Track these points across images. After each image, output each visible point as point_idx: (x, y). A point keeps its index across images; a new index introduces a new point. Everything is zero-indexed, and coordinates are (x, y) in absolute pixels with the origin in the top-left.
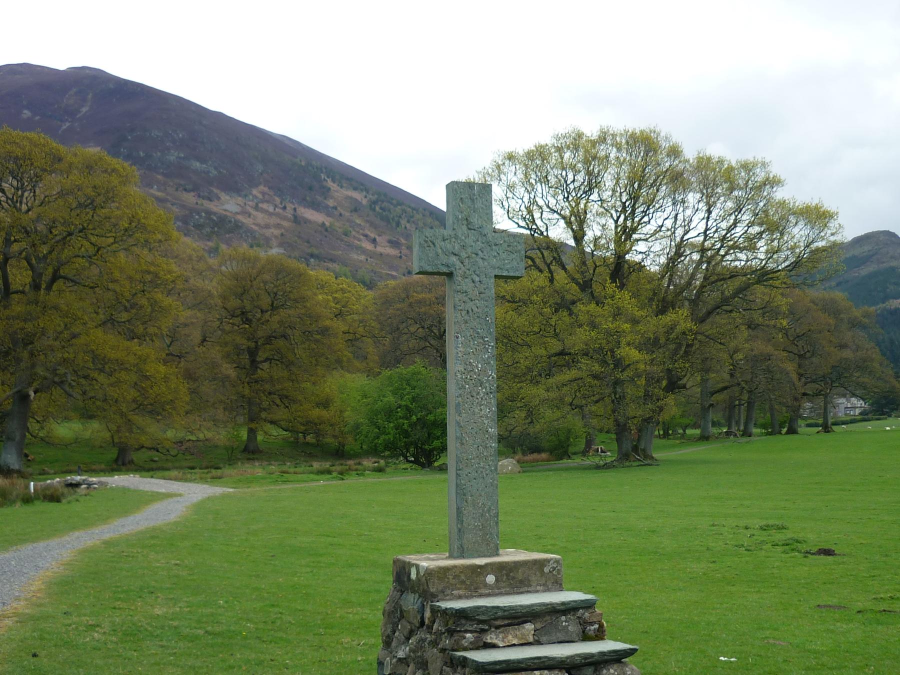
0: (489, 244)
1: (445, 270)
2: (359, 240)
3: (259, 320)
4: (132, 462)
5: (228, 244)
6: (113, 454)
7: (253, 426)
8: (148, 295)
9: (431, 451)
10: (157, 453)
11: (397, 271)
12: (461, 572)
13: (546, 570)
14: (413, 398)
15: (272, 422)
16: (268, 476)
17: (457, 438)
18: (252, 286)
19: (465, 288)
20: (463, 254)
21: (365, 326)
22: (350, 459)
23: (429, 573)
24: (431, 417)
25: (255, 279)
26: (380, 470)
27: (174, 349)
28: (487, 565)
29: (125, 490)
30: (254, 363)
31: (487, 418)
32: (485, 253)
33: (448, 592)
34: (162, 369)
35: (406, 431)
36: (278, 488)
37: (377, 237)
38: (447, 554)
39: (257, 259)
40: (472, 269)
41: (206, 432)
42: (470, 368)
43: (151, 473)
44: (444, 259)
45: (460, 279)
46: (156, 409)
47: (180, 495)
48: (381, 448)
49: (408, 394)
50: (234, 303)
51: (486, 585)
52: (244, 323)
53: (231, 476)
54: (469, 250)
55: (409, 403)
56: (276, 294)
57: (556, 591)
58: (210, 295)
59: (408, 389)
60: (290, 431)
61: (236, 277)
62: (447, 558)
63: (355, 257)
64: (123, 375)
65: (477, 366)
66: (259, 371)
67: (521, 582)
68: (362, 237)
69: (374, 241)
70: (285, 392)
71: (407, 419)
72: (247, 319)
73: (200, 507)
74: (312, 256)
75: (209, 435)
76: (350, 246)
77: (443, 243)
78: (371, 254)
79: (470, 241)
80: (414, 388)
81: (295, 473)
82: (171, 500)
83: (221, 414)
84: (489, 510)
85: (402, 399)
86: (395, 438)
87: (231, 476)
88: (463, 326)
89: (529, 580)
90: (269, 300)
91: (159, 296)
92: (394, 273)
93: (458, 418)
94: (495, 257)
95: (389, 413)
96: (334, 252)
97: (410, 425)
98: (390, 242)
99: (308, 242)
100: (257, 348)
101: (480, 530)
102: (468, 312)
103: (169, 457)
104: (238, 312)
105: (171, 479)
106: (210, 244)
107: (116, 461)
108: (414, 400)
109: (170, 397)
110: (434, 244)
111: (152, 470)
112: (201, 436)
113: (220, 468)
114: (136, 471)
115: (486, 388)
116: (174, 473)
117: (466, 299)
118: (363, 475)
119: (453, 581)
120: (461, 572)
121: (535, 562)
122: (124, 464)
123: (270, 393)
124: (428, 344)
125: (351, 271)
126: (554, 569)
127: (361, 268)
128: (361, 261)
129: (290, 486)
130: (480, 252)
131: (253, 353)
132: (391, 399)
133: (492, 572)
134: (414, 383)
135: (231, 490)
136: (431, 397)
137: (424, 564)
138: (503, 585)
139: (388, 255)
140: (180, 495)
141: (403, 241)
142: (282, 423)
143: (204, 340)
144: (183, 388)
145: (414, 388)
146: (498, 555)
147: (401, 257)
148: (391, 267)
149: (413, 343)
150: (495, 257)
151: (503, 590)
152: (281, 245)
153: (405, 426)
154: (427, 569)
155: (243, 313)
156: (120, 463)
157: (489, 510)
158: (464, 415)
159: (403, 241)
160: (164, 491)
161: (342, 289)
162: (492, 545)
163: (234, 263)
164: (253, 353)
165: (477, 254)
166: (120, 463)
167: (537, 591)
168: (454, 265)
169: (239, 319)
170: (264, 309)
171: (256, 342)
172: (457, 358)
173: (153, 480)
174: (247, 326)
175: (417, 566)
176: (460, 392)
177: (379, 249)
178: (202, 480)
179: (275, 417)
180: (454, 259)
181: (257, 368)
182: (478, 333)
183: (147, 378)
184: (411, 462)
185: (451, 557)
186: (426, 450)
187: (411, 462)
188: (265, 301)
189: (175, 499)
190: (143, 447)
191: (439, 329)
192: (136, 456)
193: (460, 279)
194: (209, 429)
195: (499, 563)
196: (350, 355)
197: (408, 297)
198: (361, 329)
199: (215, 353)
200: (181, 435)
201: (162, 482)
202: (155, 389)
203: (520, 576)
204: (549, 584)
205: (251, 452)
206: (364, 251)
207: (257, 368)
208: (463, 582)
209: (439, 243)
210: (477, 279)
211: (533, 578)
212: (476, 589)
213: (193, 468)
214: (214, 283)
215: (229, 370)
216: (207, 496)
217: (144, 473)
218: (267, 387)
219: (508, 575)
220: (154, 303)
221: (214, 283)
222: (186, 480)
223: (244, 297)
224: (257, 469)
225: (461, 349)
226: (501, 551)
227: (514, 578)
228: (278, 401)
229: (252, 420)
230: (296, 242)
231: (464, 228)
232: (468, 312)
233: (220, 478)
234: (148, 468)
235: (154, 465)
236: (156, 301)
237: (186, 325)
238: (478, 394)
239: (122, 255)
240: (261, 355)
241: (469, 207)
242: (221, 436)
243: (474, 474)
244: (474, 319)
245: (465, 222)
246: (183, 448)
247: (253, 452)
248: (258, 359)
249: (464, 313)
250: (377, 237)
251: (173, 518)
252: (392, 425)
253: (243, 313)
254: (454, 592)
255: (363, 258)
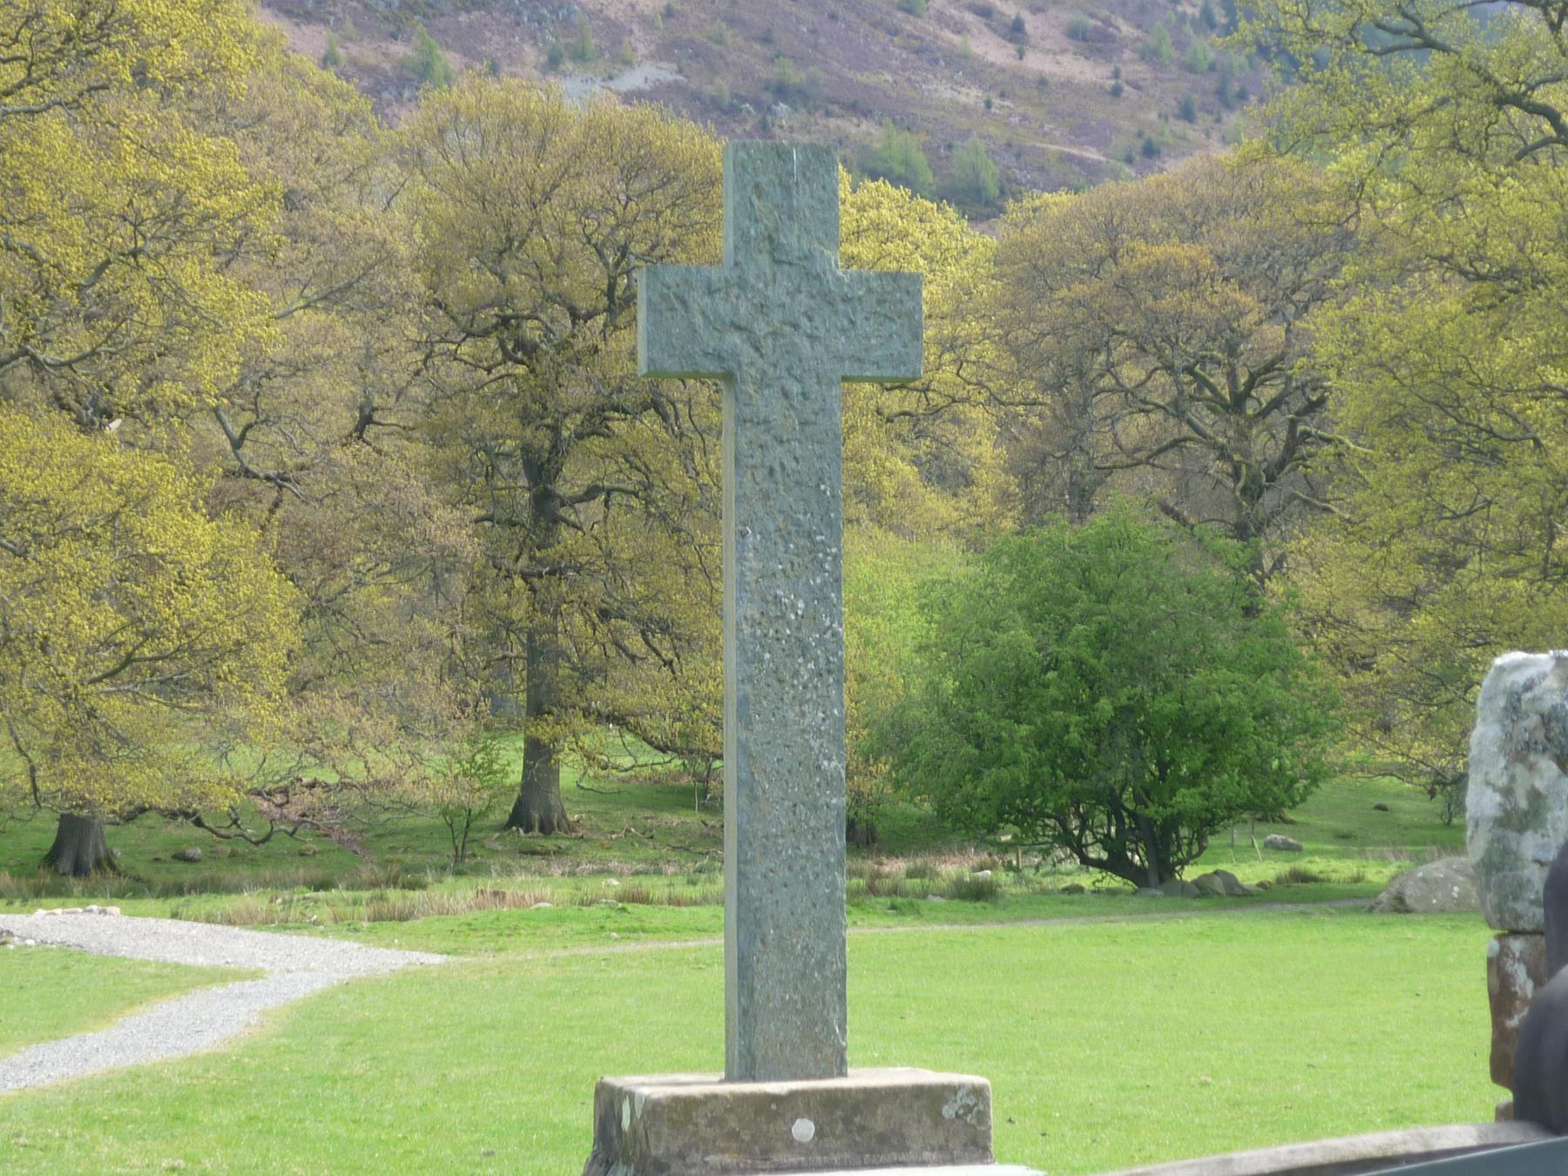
0: (826, 298)
1: (712, 366)
2: (960, 29)
3: (562, 346)
4: (106, 863)
5: (466, 52)
6: (44, 832)
7: (544, 732)
8: (151, 269)
9: (1171, 824)
10: (200, 832)
11: (1101, 143)
12: (731, 1110)
13: (948, 1111)
14: (1103, 633)
15: (618, 719)
16: (572, 911)
17: (740, 783)
18: (536, 222)
19: (763, 412)
20: (761, 328)
21: (960, 363)
22: (893, 854)
23: (655, 1109)
24: (1167, 705)
25: (547, 197)
26: (978, 893)
27: (260, 455)
28: (793, 1095)
29: (71, 954)
30: (545, 503)
31: (819, 733)
32: (817, 322)
33: (695, 1157)
34: (203, 530)
35: (1078, 754)
36: (603, 951)
37: (1026, 16)
38: (723, 1075)
39: (550, 126)
40: (783, 364)
41: (372, 755)
42: (773, 611)
43: (174, 902)
44: (710, 340)
45: (751, 389)
46: (184, 673)
47: (255, 975)
48: (986, 814)
49: (1085, 617)
50: (472, 281)
51: (791, 1144)
52: (508, 356)
53: (443, 911)
54: (776, 317)
55: (1086, 654)
56: (624, 251)
57: (971, 1161)
58: (387, 258)
59: (1085, 601)
60: (679, 752)
61: (481, 194)
62: (721, 1082)
63: (944, 92)
64: (67, 554)
65: (794, 607)
66: (565, 533)
67: (882, 1139)
68: (969, 17)
69: (1015, 32)
70: (660, 611)
71: (1081, 708)
72: (520, 344)
73: (313, 1018)
74: (782, 91)
75: (384, 764)
76: (926, 54)
77: (707, 300)
78: (1002, 84)
79: (778, 294)
80: (1106, 597)
81: (675, 902)
82: (217, 989)
83: (434, 696)
84: (821, 965)
85: (1061, 637)
86: (1035, 776)
87: (443, 911)
88: (758, 507)
89: (903, 1136)
90: (599, 276)
91: (189, 272)
92: (1092, 154)
93: (744, 735)
94: (843, 330)
95: (1017, 688)
96: (862, 78)
97: (1094, 732)
98: (1074, 33)
99: (766, 40)
100: (557, 448)
101: (798, 1012)
102: (771, 471)
103: (241, 847)
104: (489, 316)
105: (230, 922)
106: (399, 49)
107: (52, 858)
108: (1102, 640)
109: (235, 633)
110: (684, 303)
111: (179, 890)
112: (356, 771)
113: (423, 887)
114: (120, 894)
115: (816, 660)
116: (252, 900)
117: (766, 438)
118: (917, 912)
119: (708, 1133)
120: (731, 1110)
121: (919, 1092)
122: (79, 870)
123: (604, 615)
124: (1186, 429)
125: (926, 148)
126: (968, 1109)
127: (965, 135)
128: (965, 110)
129: (648, 946)
130: (804, 321)
131: (541, 470)
132: (1020, 636)
133: (807, 1113)
134: (1104, 580)
135: (437, 959)
136: (1168, 626)
137: (645, 1091)
138: (835, 1144)
139: (1067, 84)
140: (255, 975)
141: (1126, 29)
142: (646, 722)
143: (366, 420)
144: (279, 595)
145: (1106, 597)
146: (843, 1074)
147: (1116, 92)
148: (1082, 131)
149: (1135, 428)
150: (843, 330)
151: (836, 1159)
152: (665, 51)
153: (1074, 736)
154: (647, 1098)
155: (505, 321)
156: (66, 864)
157: (821, 965)
158: (759, 727)
159: (1126, 29)
160: (201, 960)
161: (877, 227)
162: (828, 1051)
163: (471, 141)
164: (541, 470)
165: (796, 326)
166: (66, 864)
167: (923, 1163)
168: (735, 355)
169: (493, 342)
170: (583, 306)
171: (555, 429)
172: (742, 585)
173: (181, 926)
174: (521, 370)
175: (631, 1095)
176: (752, 669)
177: (1036, 63)
178: (343, 924)
179: (628, 701)
180: (735, 339)
181: (556, 520)
182: (798, 524)
183: (153, 564)
184: (1098, 864)
185: (729, 1078)
186: (1150, 822)
187: (1098, 864)
188: (585, 278)
189: (235, 987)
190: (143, 810)
191: (1232, 376)
192: (120, 843)
193: (751, 389)
194: (381, 744)
195: (828, 1091)
196: (909, 472)
197: (1113, 254)
198: (948, 373)
199: (403, 464)
200: (283, 761)
201: (200, 929)
202: (183, 601)
203: (879, 1123)
204: (956, 1145)
205: (533, 822)
206: (976, 72)
207: (556, 520)
208: (733, 1135)
209: (698, 300)
210: (795, 388)
211: (913, 1132)
212: (766, 1154)
213: (324, 885)
214: (399, 216)
215: (454, 529)
216: (346, 977)
217: (150, 904)
218: (595, 588)
219: (847, 1121)
220: (172, 295)
221: (399, 216)
222: (284, 925)
223: (507, 262)
224: (542, 888)
225: (754, 564)
226: (850, 1070)
227: (862, 1129)
228: (635, 643)
229: (537, 710)
230: (720, 41)
231: (764, 260)
232: (771, 471)
233: (403, 917)
234: (135, 887)
235: (187, 875)
236: (179, 291)
237: (297, 369)
238: (796, 674)
239: (54, 127)
240: (573, 478)
241: (777, 207)
242: (428, 768)
243: (783, 874)
244: (788, 489)
245: (766, 245)
246: (293, 811)
247: (546, 829)
248: (563, 489)
249: (761, 474)
250: (1026, 16)
251: (207, 1043)
252: (1024, 730)
253: (505, 321)
254: (710, 1159)
255: (972, 96)
